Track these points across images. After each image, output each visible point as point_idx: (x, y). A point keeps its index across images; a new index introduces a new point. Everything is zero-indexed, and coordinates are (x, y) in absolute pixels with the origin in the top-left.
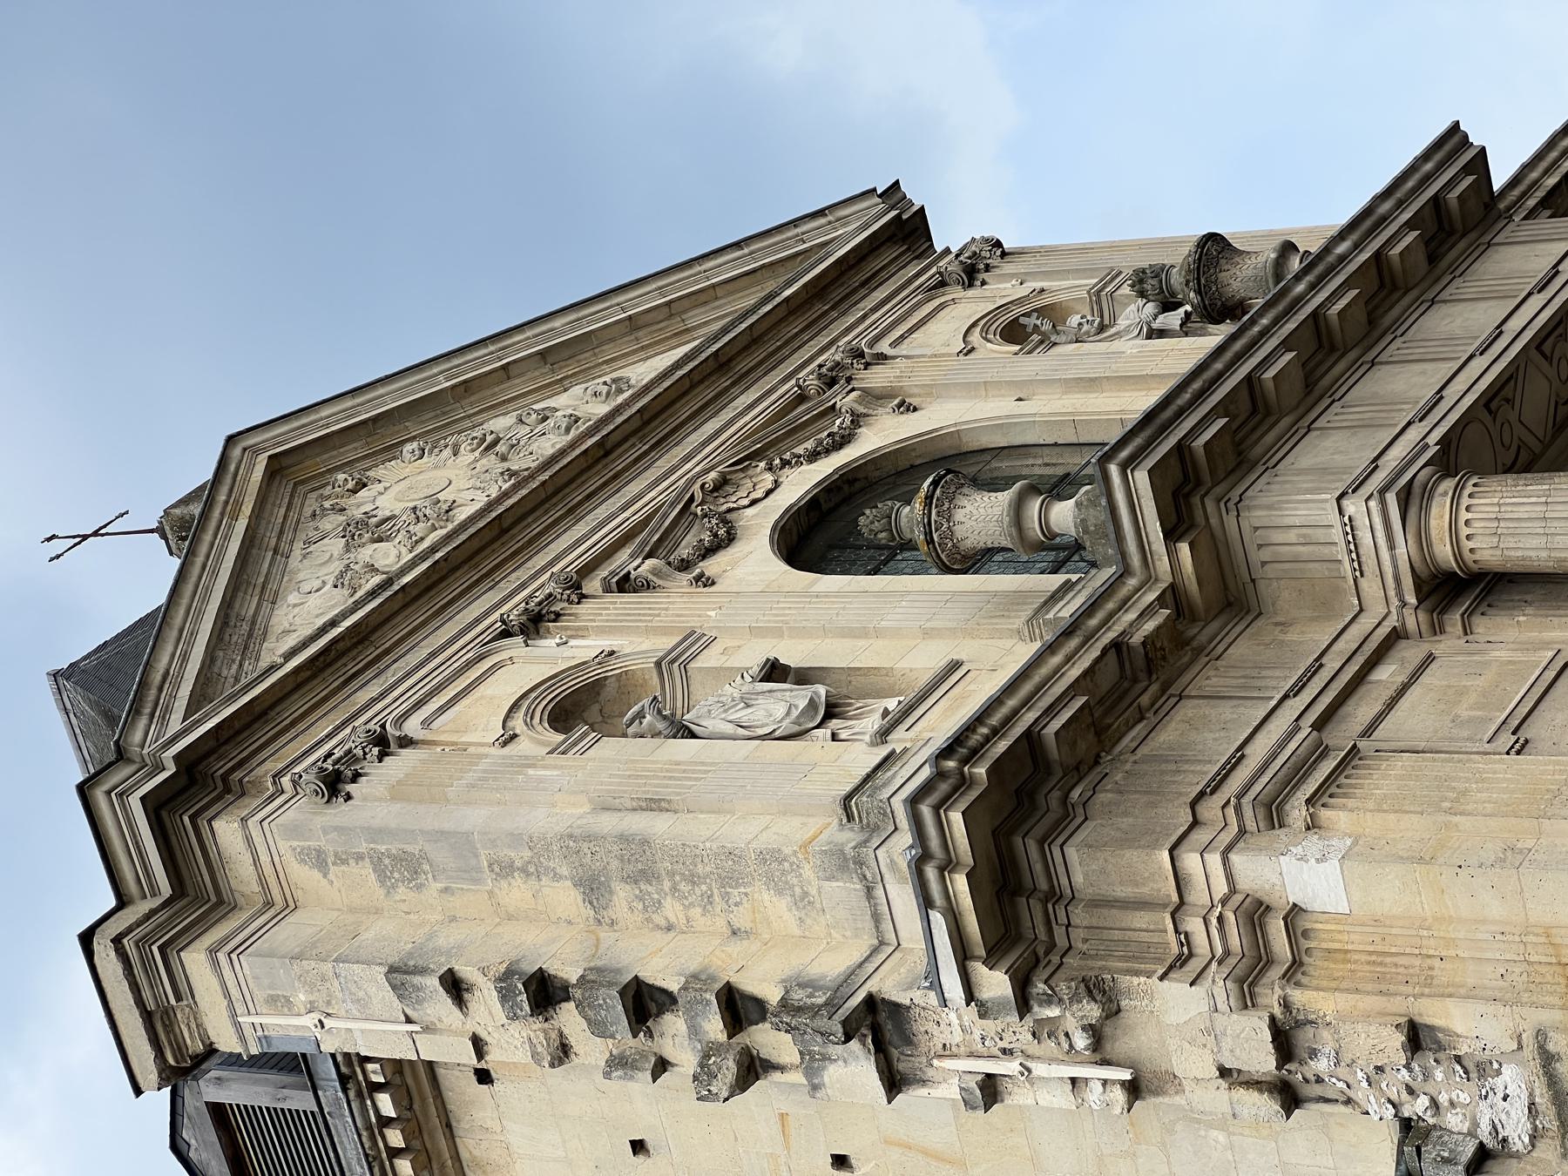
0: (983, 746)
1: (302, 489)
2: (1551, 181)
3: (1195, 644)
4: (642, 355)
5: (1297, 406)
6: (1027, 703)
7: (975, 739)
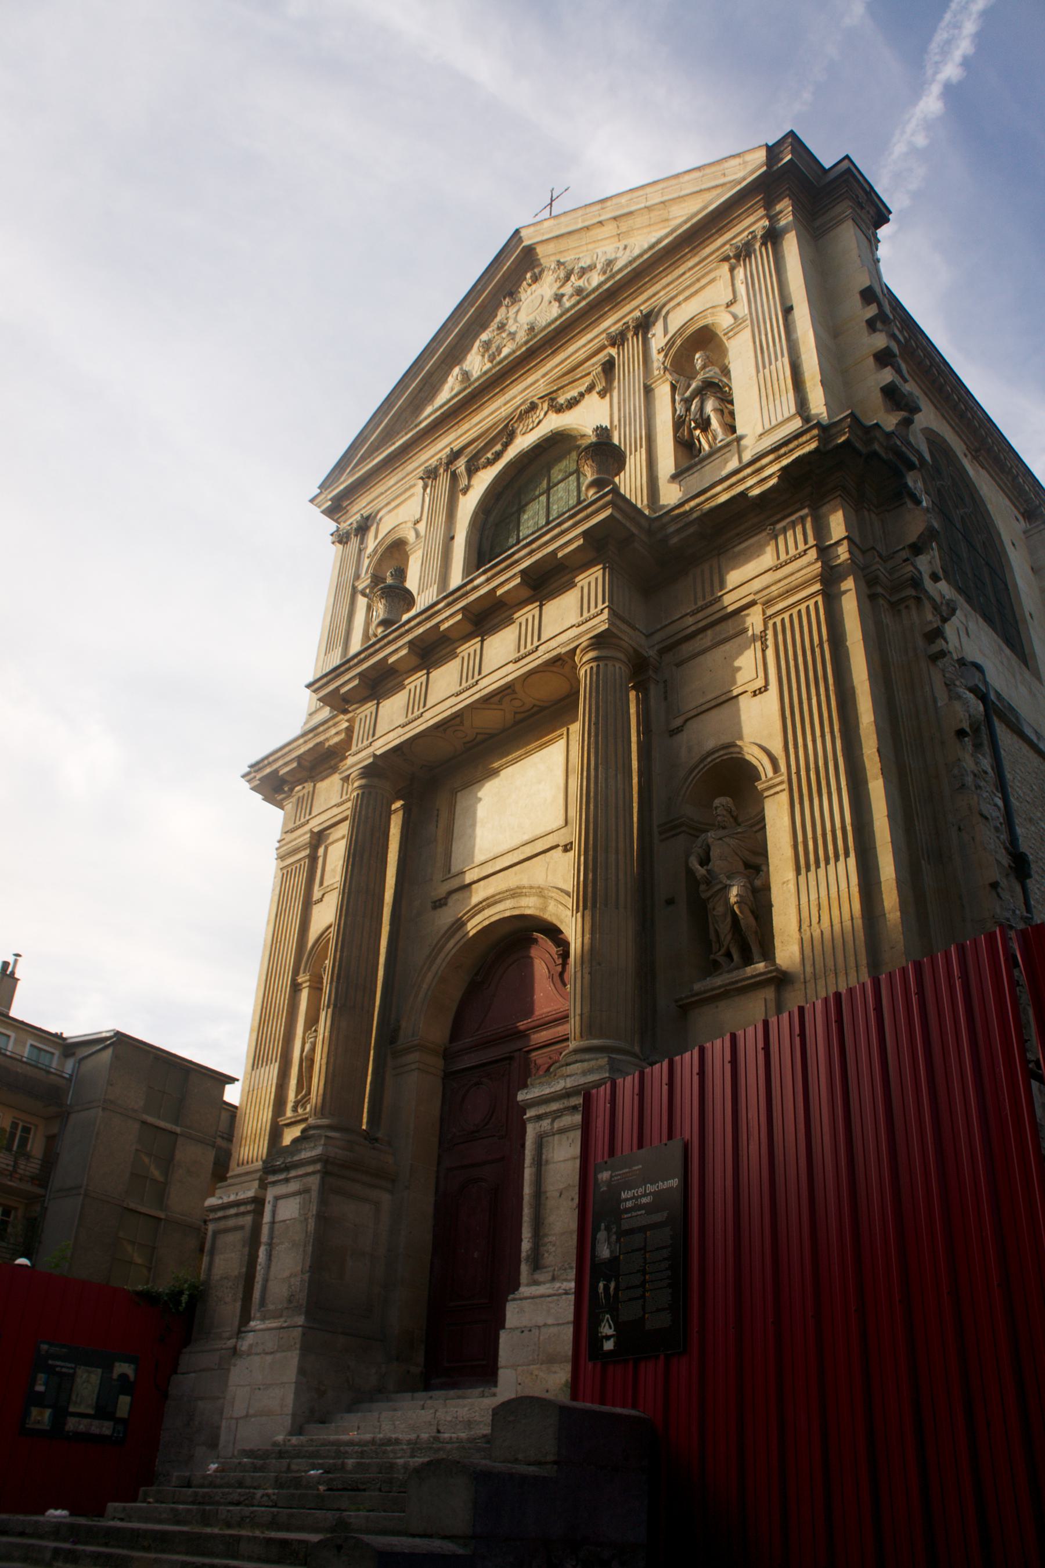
2: (724, 498)
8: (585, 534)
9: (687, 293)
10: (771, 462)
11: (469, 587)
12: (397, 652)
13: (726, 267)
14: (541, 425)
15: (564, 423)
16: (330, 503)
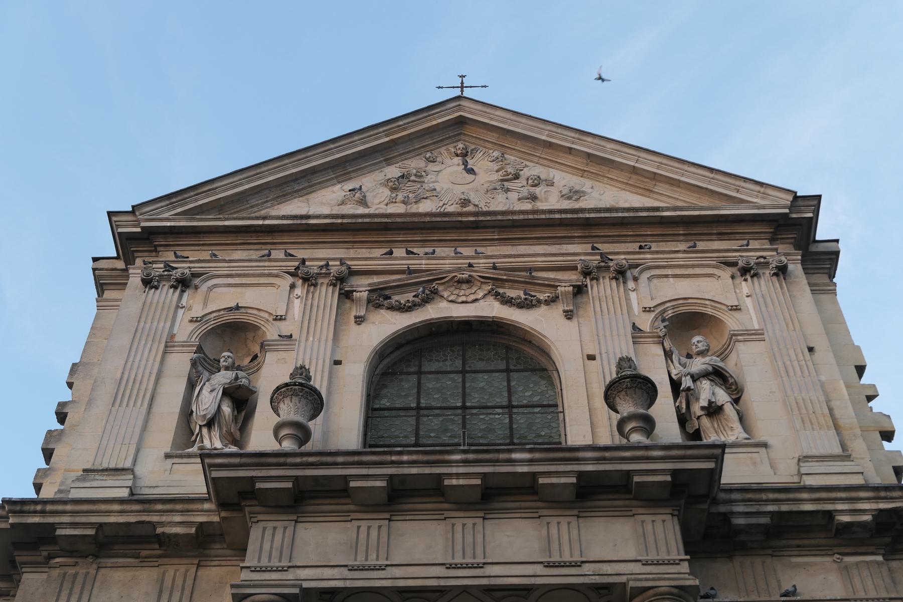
0: (29, 512)
2: (808, 507)
3: (207, 552)
4: (623, 186)
5: (367, 506)
6: (73, 513)
7: (27, 508)
8: (675, 473)
10: (868, 499)
12: (372, 479)
14: (474, 304)
15: (513, 318)
16: (139, 230)
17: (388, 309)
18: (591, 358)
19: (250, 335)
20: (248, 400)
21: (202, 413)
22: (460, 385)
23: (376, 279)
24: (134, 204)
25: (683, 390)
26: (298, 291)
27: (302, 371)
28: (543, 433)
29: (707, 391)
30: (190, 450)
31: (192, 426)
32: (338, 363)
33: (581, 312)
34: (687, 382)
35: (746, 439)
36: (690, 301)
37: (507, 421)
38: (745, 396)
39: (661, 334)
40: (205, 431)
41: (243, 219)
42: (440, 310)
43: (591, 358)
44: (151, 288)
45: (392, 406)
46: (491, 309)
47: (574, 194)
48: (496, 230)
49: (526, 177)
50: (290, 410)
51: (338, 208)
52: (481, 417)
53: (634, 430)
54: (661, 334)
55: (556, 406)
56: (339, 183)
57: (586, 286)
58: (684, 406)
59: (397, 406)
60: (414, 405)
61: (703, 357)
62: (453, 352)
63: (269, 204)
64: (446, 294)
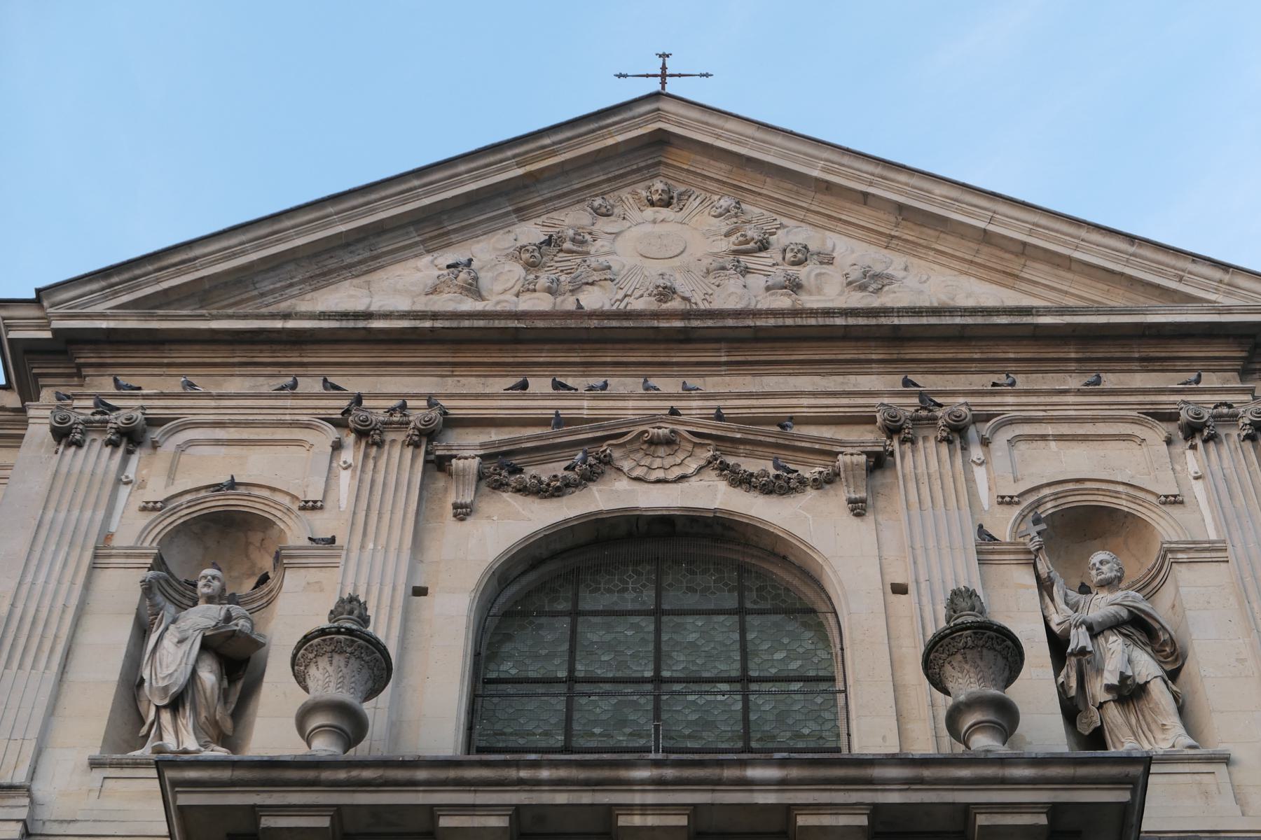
1: (662, 170)
8: (1054, 810)
9: (1065, 429)
11: (728, 773)
13: (333, 433)
16: (47, 335)
17: (518, 491)
18: (900, 589)
19: (256, 537)
20: (248, 660)
21: (162, 684)
22: (651, 637)
23: (495, 435)
24: (40, 286)
25: (1072, 654)
26: (347, 455)
27: (352, 607)
28: (806, 731)
29: (1117, 657)
30: (138, 753)
31: (143, 708)
32: (420, 592)
33: (881, 503)
34: (1079, 639)
35: (1191, 747)
36: (1088, 485)
37: (739, 706)
38: (1190, 667)
39: (1032, 547)
40: (166, 717)
41: (245, 317)
42: (614, 495)
43: (900, 589)
44: (69, 445)
45: (523, 675)
46: (711, 494)
47: (872, 280)
48: (723, 345)
49: (782, 246)
50: (328, 681)
51: (424, 299)
52: (690, 698)
53: (978, 727)
54: (1032, 547)
55: (832, 679)
56: (428, 252)
57: (892, 454)
58: (1073, 683)
59: (532, 675)
60: (562, 674)
61: (1111, 591)
62: (639, 574)
63: (295, 290)
64: (626, 465)
